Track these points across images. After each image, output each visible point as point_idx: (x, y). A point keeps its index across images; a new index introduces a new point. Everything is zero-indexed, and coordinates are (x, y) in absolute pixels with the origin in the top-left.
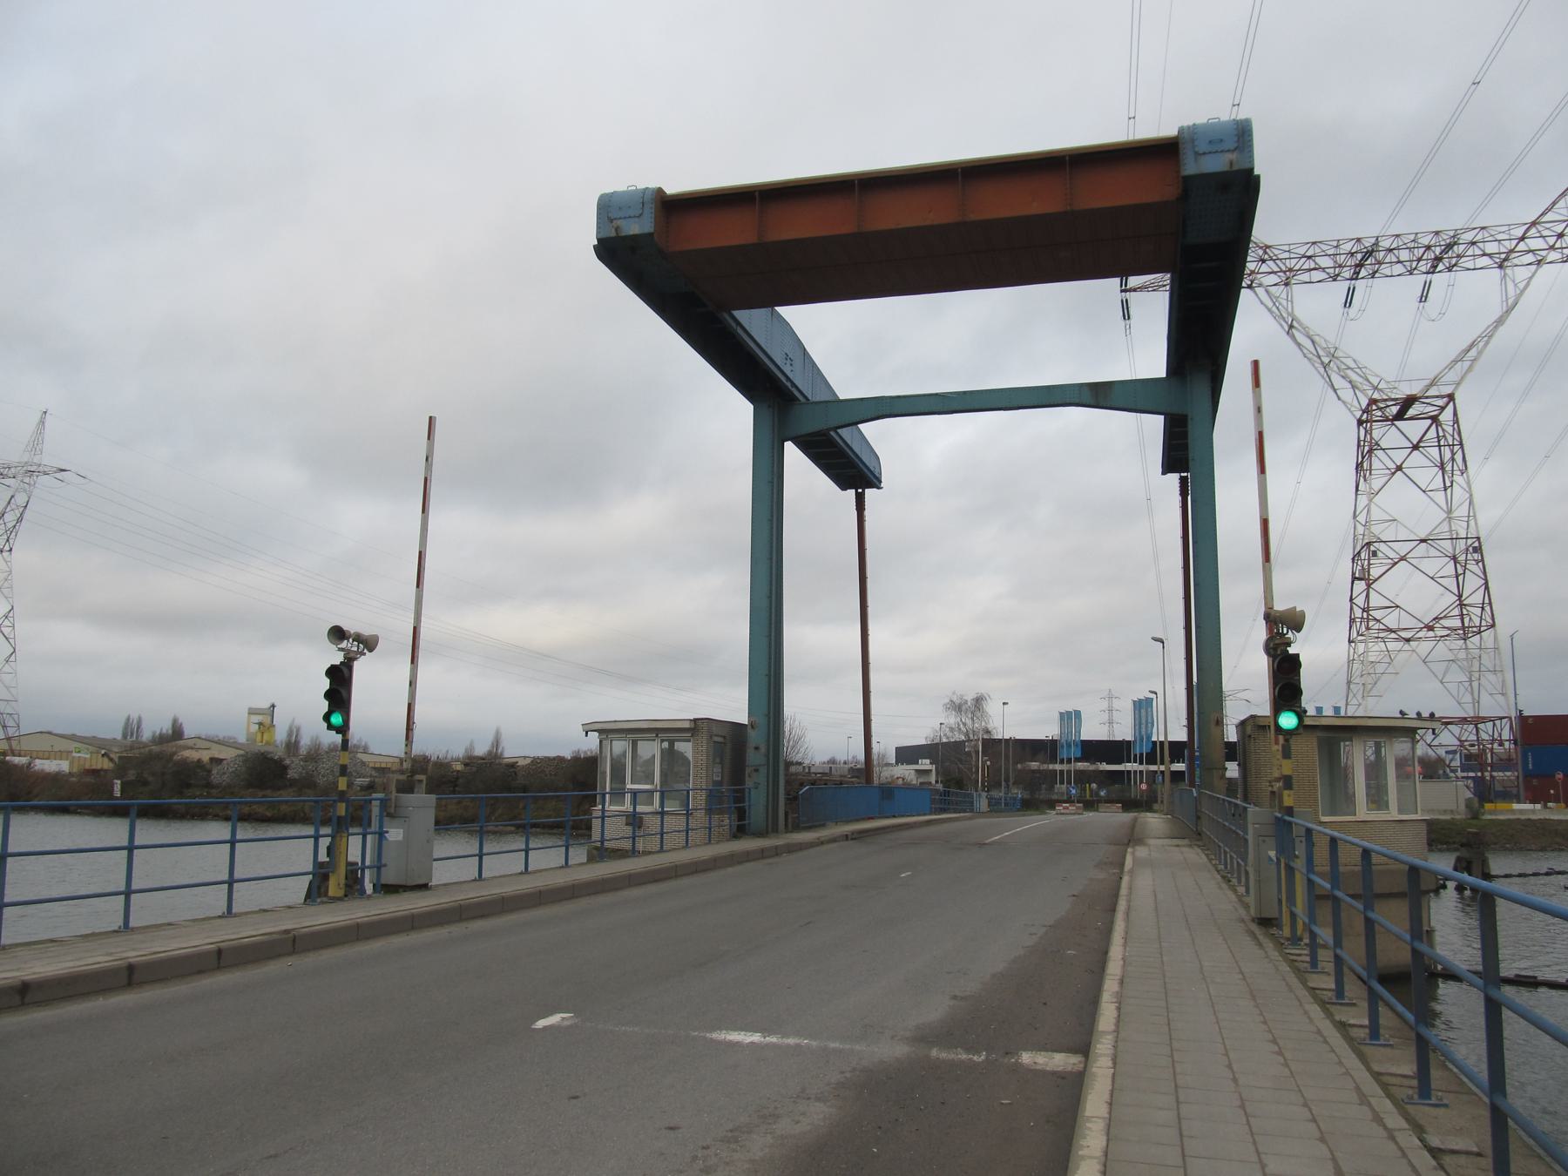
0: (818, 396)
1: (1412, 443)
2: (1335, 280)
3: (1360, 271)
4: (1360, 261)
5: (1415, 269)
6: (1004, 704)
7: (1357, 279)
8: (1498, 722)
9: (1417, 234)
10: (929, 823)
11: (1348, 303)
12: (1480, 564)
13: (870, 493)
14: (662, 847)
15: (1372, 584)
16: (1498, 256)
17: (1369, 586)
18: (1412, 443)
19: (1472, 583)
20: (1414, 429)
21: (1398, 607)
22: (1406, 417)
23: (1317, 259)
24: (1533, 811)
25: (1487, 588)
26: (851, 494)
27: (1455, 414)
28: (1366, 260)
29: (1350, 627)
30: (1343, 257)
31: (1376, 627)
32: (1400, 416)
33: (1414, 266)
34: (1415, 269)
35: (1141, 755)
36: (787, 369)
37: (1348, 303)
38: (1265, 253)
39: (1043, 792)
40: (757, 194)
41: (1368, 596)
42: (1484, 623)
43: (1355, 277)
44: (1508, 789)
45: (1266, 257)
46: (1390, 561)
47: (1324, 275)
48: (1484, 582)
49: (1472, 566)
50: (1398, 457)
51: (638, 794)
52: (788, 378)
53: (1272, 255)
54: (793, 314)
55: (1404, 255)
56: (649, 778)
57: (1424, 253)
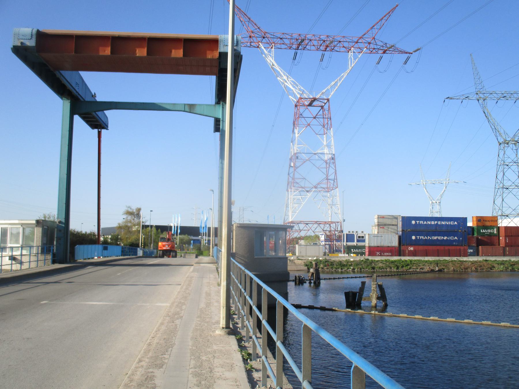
0: (88, 99)
1: (313, 116)
2: (290, 49)
3: (299, 47)
4: (299, 43)
5: (319, 49)
6: (151, 211)
7: (298, 49)
8: (337, 224)
9: (320, 35)
10: (127, 259)
11: (295, 58)
12: (334, 164)
13: (103, 131)
14: (395, 225)
15: (296, 169)
16: (348, 48)
17: (295, 170)
18: (313, 116)
19: (331, 171)
20: (314, 110)
21: (304, 178)
22: (312, 105)
23: (284, 40)
24: (344, 257)
25: (336, 173)
26: (96, 131)
27: (329, 107)
28: (301, 43)
29: (453, 99)
30: (293, 40)
31: (297, 186)
32: (310, 105)
33: (318, 47)
34: (319, 49)
35: (206, 233)
36: (77, 88)
37: (295, 58)
38: (265, 35)
39: (248, 368)
40: (74, 36)
41: (294, 174)
42: (334, 187)
43: (298, 49)
44: (339, 249)
45: (265, 36)
46: (302, 160)
47: (286, 47)
48: (335, 171)
49: (332, 166)
50: (309, 120)
51: (14, 249)
52: (77, 92)
53: (267, 36)
54: (84, 74)
55: (315, 43)
56: (17, 242)
57: (323, 43)
